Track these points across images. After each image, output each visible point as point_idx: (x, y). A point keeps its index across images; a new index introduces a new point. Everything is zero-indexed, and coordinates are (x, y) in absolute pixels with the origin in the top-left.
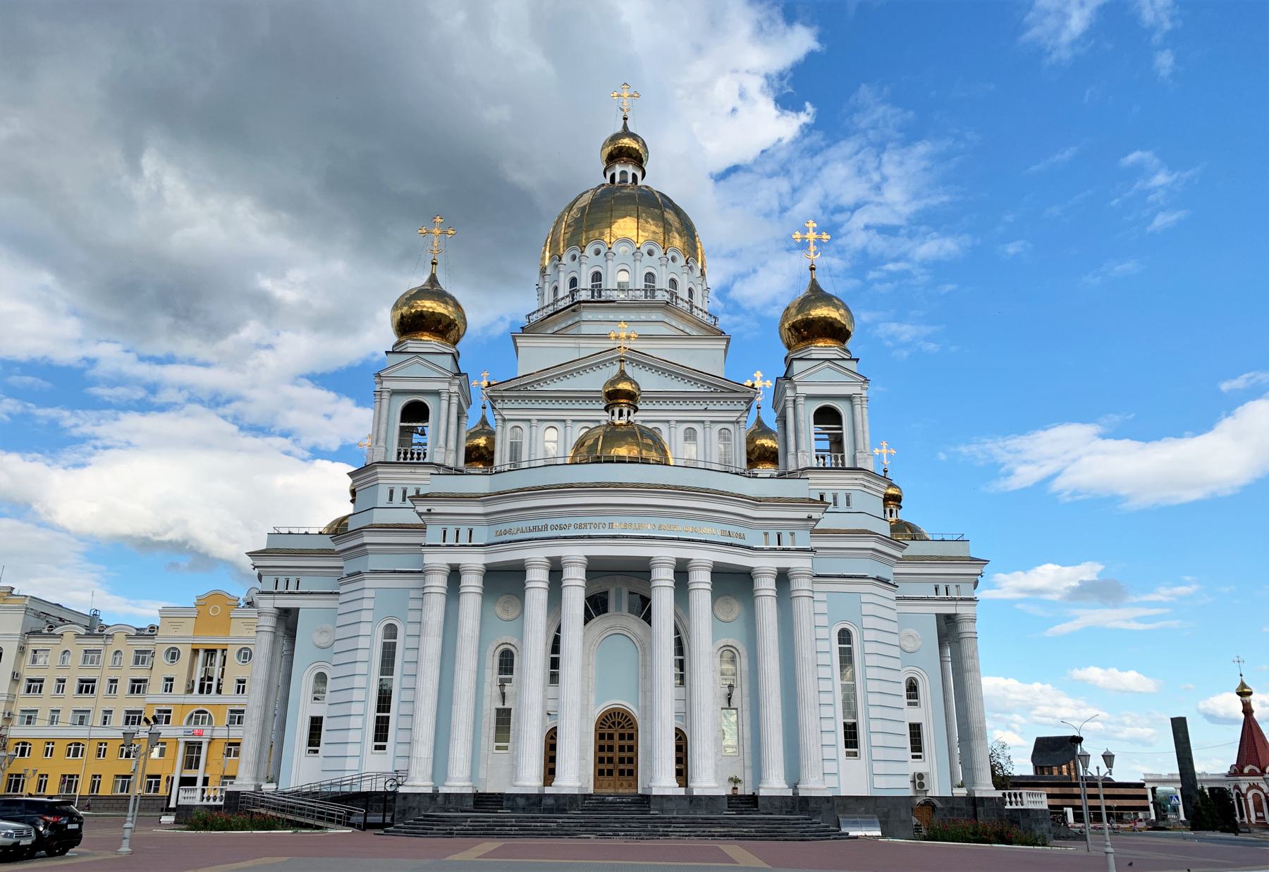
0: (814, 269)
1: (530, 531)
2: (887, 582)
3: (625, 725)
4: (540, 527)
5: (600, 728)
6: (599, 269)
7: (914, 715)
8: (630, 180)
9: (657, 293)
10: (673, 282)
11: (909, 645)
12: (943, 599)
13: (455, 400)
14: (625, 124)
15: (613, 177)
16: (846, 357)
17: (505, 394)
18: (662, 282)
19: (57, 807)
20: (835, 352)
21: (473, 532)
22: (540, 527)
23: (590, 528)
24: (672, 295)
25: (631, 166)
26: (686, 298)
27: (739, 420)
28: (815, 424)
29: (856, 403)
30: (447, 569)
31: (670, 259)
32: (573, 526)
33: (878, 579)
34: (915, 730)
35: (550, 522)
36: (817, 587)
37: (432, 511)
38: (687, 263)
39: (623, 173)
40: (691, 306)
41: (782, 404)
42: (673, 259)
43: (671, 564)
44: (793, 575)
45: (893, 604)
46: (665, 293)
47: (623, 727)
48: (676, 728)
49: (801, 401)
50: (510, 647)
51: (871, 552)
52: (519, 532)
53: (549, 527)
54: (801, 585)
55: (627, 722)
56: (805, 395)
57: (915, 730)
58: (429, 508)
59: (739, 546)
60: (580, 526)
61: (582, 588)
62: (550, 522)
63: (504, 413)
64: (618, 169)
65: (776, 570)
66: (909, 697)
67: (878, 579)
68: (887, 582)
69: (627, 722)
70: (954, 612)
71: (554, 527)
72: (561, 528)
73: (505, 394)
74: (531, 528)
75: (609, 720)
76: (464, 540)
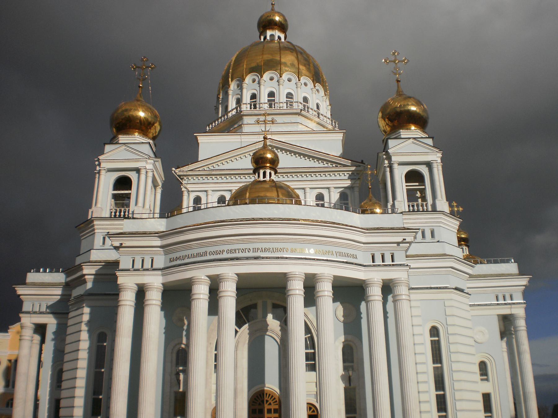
0: (400, 81)
1: (194, 257)
2: (462, 290)
3: (272, 403)
4: (201, 254)
5: (252, 405)
6: (255, 92)
7: (486, 387)
8: (277, 38)
9: (294, 104)
10: (305, 100)
11: (479, 338)
12: (502, 304)
13: (150, 174)
14: (273, 7)
15: (265, 38)
16: (424, 136)
17: (190, 173)
18: (298, 97)
19: (525, 302)
20: (417, 133)
21: (76, 226)
22: (201, 254)
23: (239, 253)
24: (304, 106)
25: (277, 31)
26: (315, 108)
27: (353, 186)
28: (406, 182)
29: (435, 167)
30: (136, 288)
31: (303, 84)
32: (225, 251)
33: (456, 289)
34: (487, 398)
35: (209, 249)
36: (413, 297)
37: (124, 245)
38: (315, 87)
39: (272, 36)
40: (318, 114)
41: (383, 170)
42: (306, 84)
43: (301, 278)
44: (397, 283)
45: (469, 308)
46: (300, 104)
47: (270, 404)
48: (308, 403)
49: (396, 166)
50: (351, 343)
51: (450, 269)
52: (186, 258)
53: (208, 253)
54: (402, 291)
55: (271, 398)
56: (398, 162)
57: (487, 398)
58: (121, 242)
59: (352, 264)
60: (231, 251)
61: (234, 298)
62: (209, 249)
63: (188, 186)
64: (269, 33)
65: (381, 281)
66: (482, 375)
67: (456, 289)
68: (462, 290)
69: (271, 398)
70: (510, 313)
71: (211, 253)
72: (217, 253)
73: (190, 173)
74: (195, 255)
75: (272, 400)
76: (388, 261)
